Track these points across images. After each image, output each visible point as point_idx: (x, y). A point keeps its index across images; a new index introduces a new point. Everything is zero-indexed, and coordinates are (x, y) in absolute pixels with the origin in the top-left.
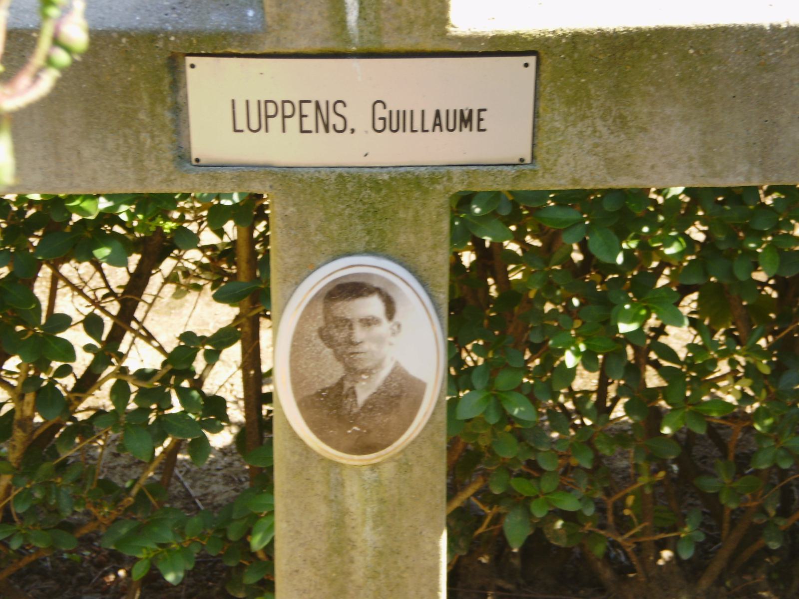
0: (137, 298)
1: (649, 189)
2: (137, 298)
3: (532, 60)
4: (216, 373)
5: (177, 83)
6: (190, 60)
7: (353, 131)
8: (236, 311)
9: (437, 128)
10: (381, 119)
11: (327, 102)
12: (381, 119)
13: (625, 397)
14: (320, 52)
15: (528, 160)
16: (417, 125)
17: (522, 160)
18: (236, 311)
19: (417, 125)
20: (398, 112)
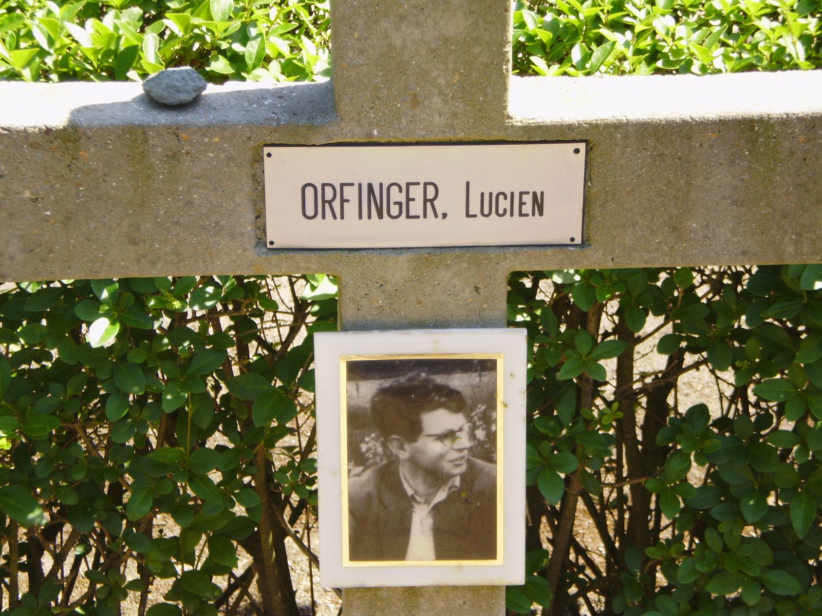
0: (254, 331)
1: (229, 276)
2: (254, 331)
3: (582, 147)
4: (359, 356)
5: (258, 159)
6: (267, 150)
7: (445, 216)
8: (664, 316)
10: (395, 203)
11: (381, 185)
12: (395, 203)
13: (105, 391)
14: (150, 105)
15: (578, 241)
17: (572, 240)
18: (664, 316)
20: (491, 194)
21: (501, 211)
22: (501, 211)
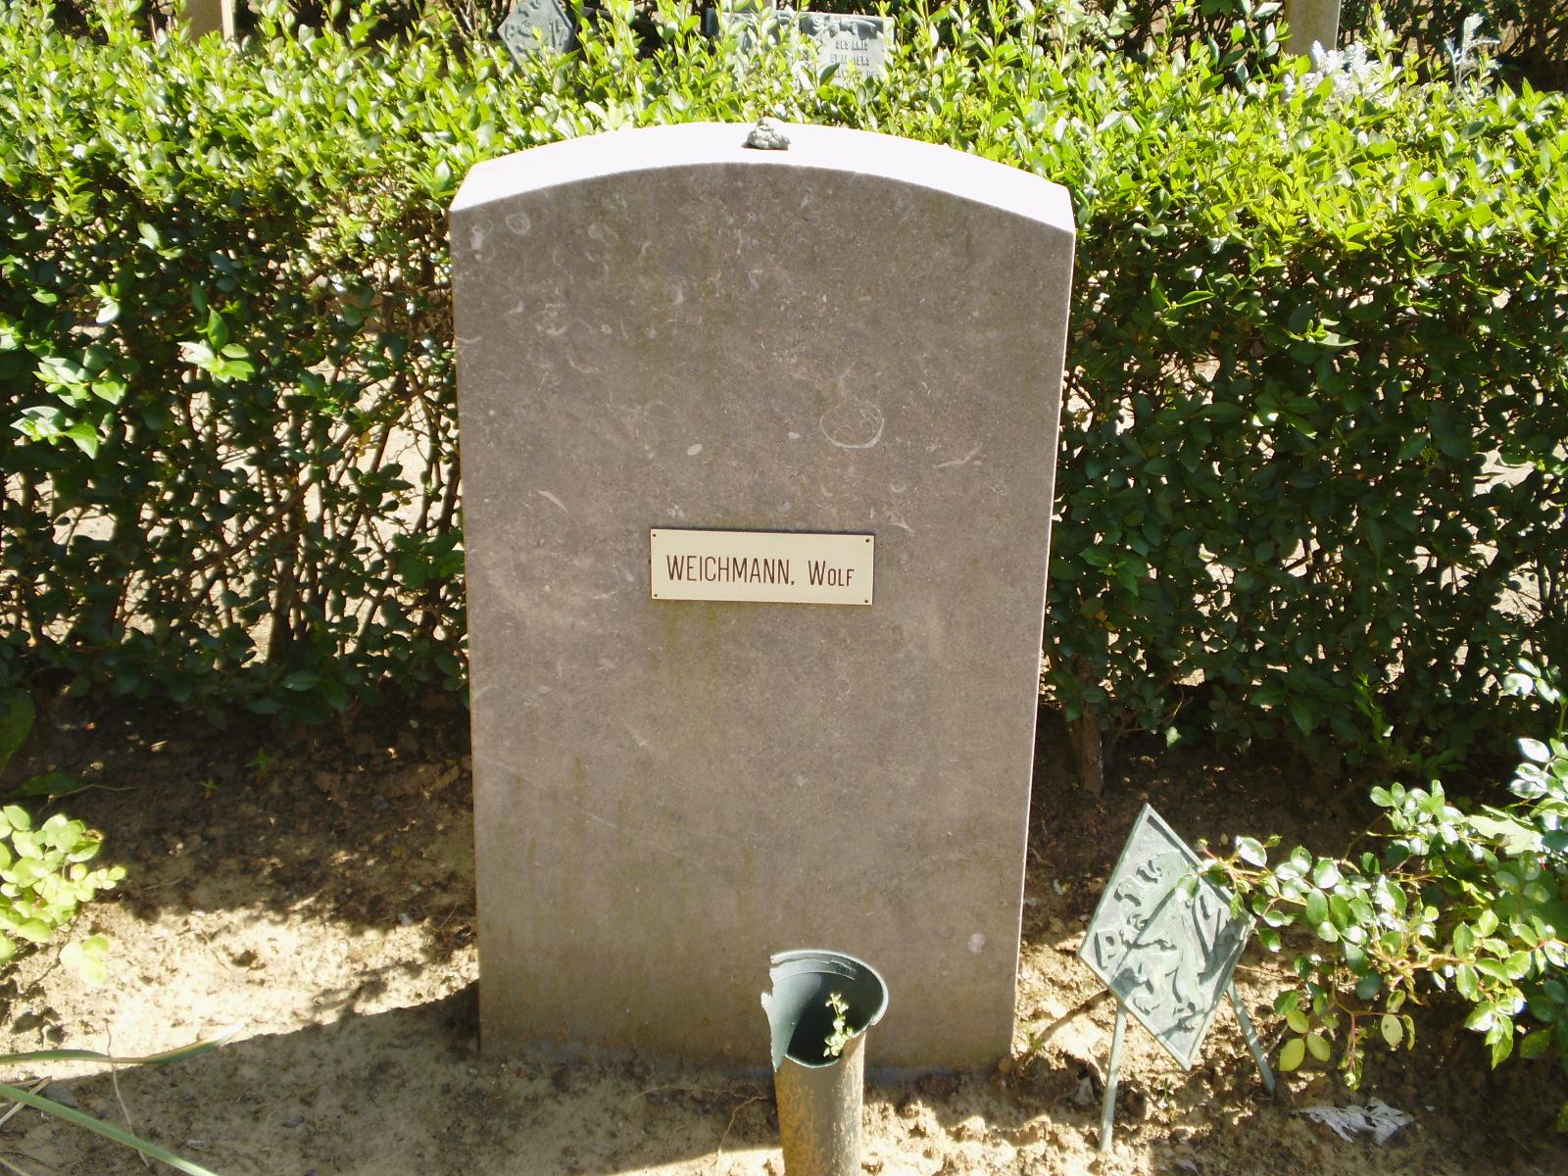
3: (872, 538)
6: (653, 531)
9: (755, 578)
16: (844, 580)
19: (844, 580)
21: (710, 577)
22: (710, 577)
